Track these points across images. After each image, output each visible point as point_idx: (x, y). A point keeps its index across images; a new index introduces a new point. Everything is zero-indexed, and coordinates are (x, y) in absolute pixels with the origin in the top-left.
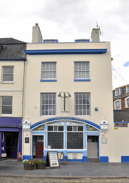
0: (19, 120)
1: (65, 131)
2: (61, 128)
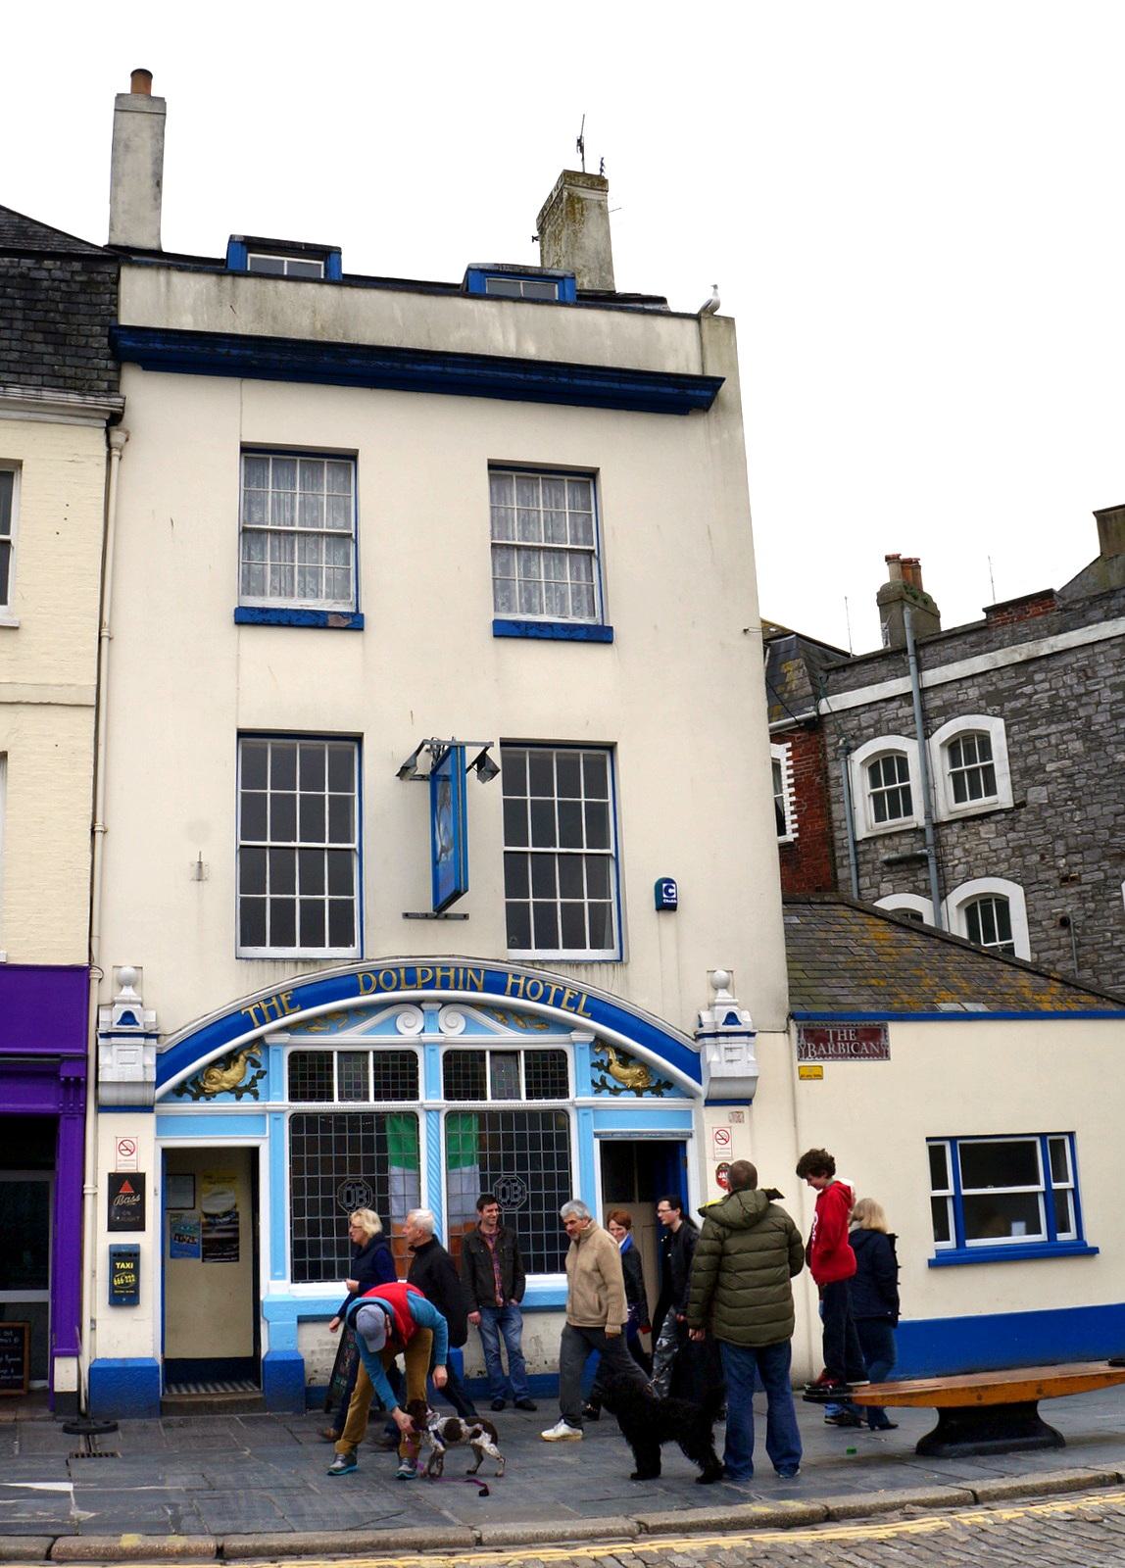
1: (431, 1096)
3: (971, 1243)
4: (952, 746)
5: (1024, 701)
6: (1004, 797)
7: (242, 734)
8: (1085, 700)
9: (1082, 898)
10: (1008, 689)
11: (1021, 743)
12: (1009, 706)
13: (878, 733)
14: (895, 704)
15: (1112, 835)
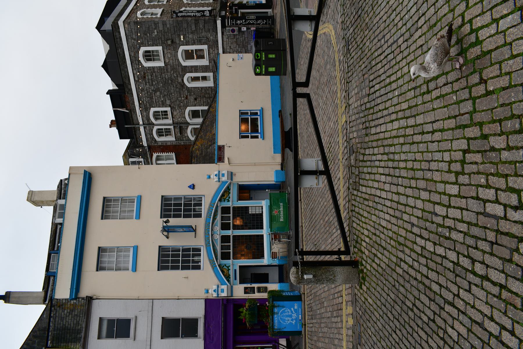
0: (209, 303)
1: (229, 233)
2: (225, 239)
3: (259, 131)
4: (156, 119)
5: (147, 103)
6: (168, 109)
7: (158, 270)
8: (148, 91)
9: (190, 95)
10: (144, 106)
11: (157, 105)
12: (148, 106)
13: (152, 134)
14: (146, 130)
15: (178, 88)
